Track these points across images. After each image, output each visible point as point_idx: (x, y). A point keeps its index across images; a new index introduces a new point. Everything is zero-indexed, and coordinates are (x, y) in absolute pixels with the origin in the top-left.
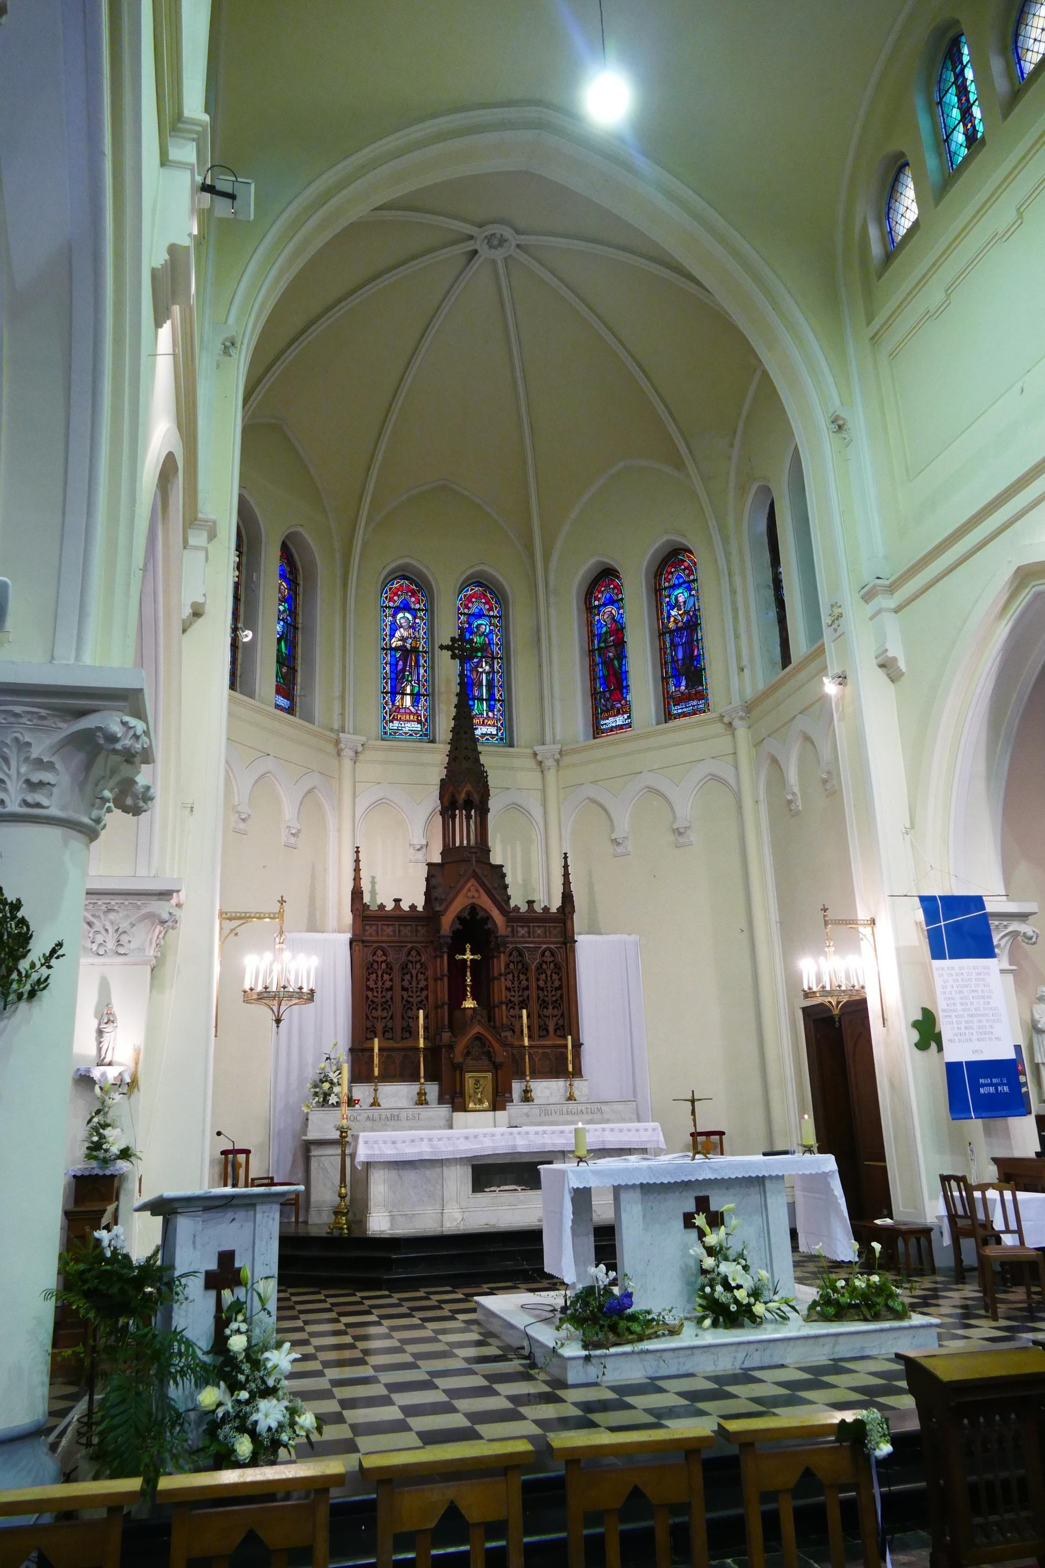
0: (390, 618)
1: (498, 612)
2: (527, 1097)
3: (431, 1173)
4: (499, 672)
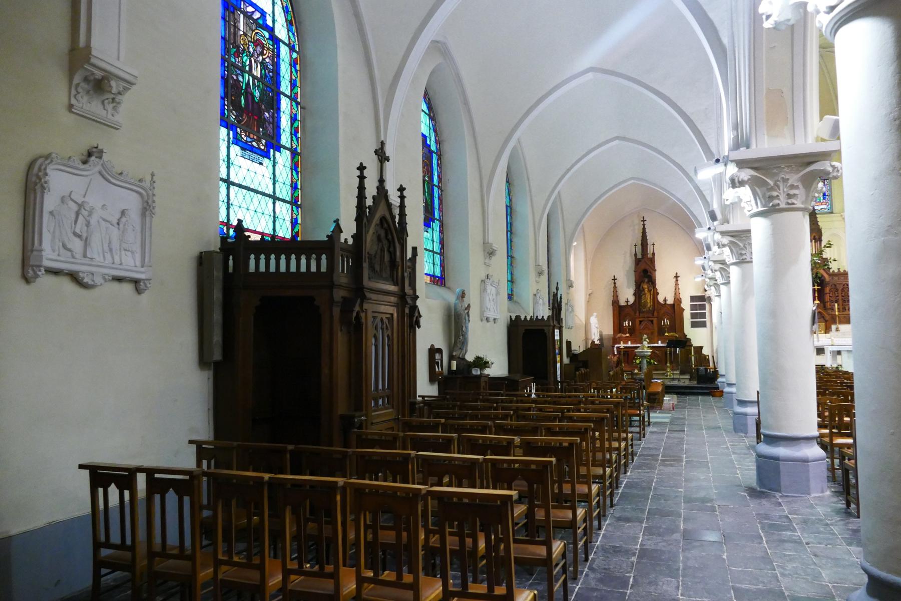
2: (837, 330)
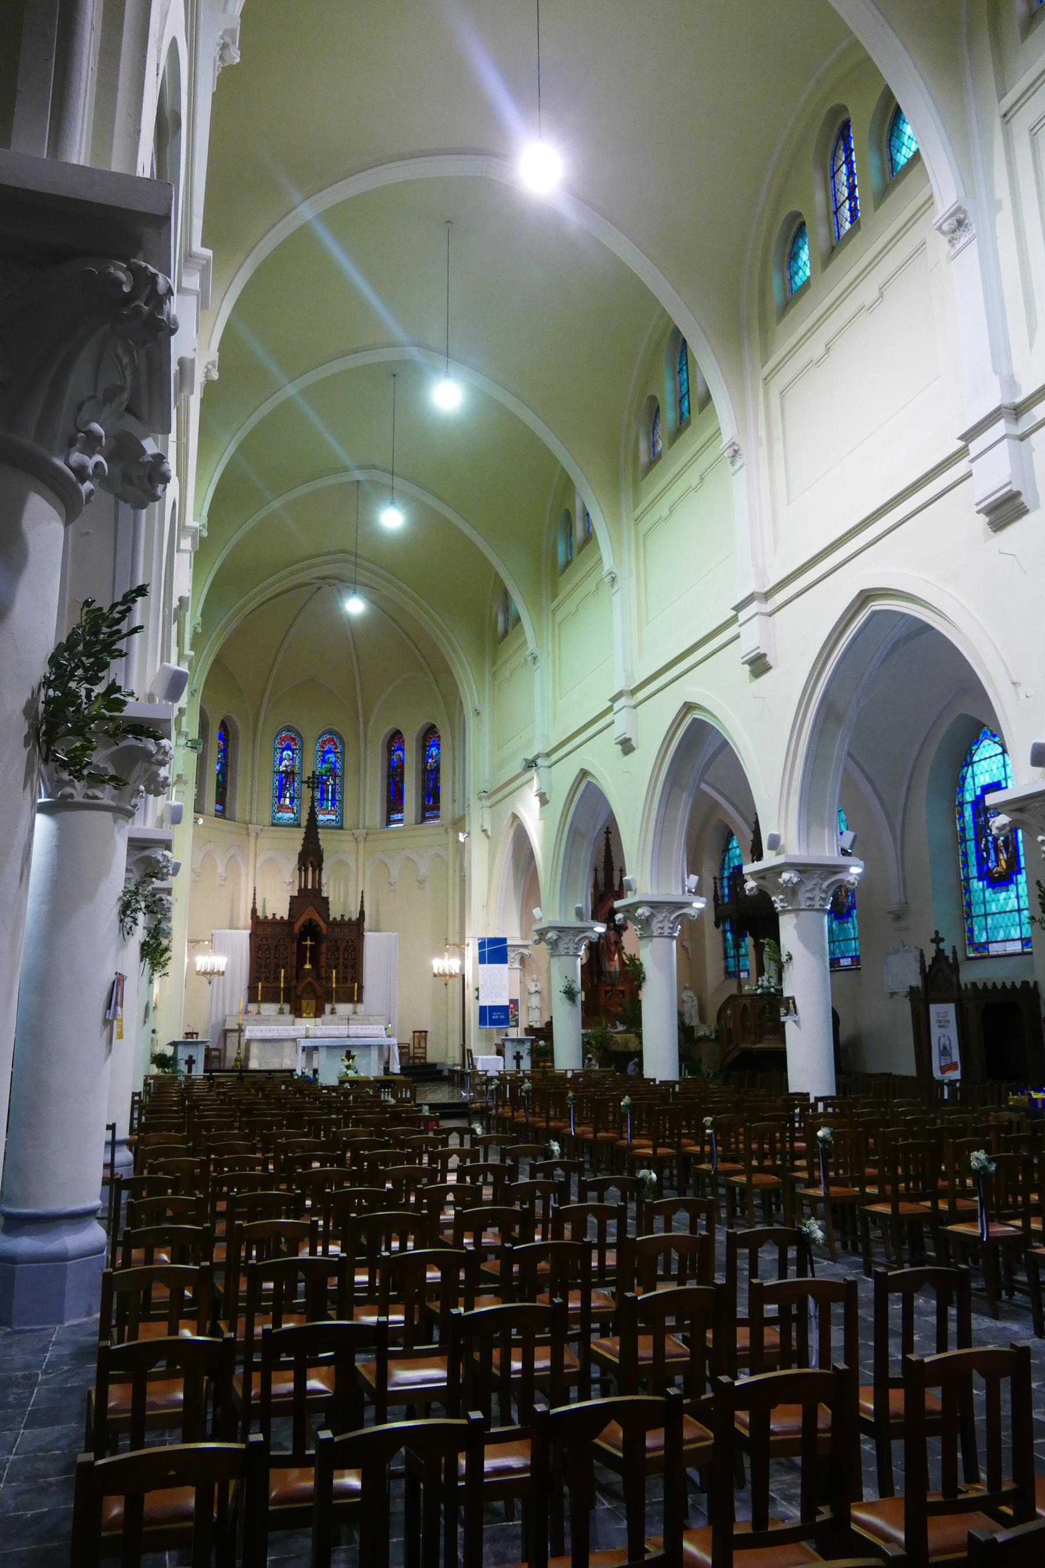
2: (333, 1012)
3: (277, 1045)
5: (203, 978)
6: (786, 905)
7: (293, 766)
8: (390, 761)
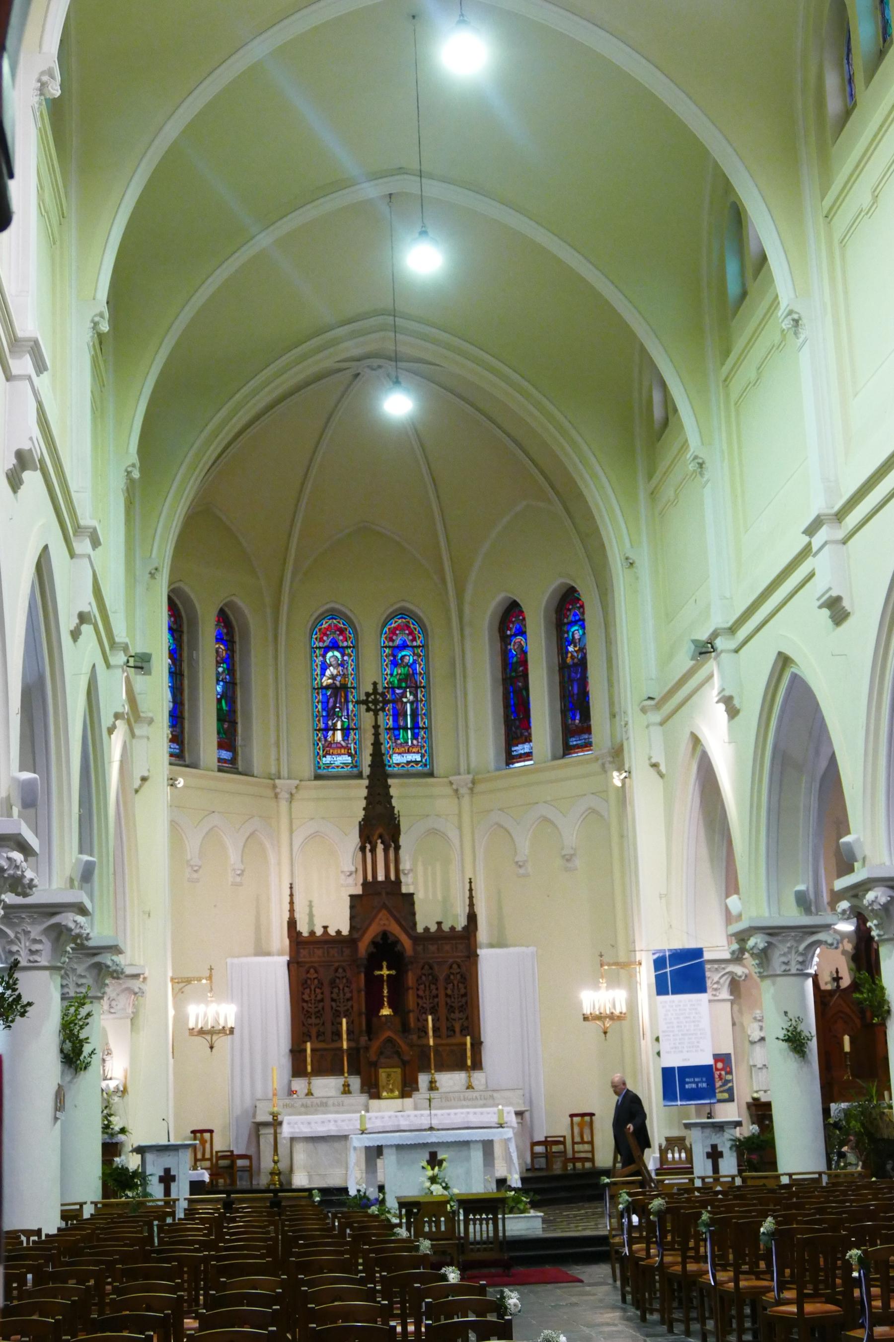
0: (321, 658)
1: (421, 642)
2: (432, 1086)
3: (337, 1145)
4: (422, 700)
5: (199, 1039)
6: (762, 970)
7: (344, 676)
8: (505, 654)
